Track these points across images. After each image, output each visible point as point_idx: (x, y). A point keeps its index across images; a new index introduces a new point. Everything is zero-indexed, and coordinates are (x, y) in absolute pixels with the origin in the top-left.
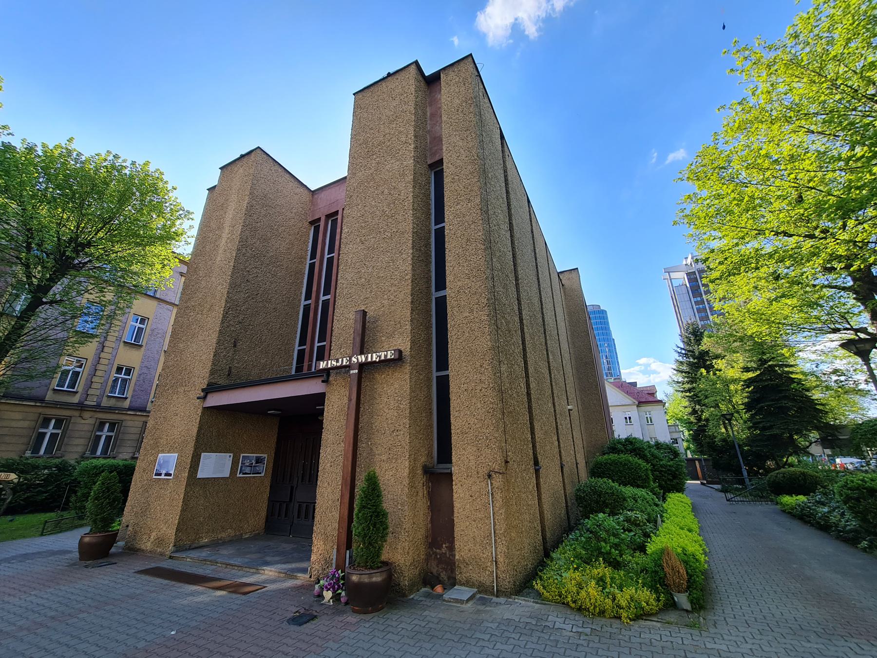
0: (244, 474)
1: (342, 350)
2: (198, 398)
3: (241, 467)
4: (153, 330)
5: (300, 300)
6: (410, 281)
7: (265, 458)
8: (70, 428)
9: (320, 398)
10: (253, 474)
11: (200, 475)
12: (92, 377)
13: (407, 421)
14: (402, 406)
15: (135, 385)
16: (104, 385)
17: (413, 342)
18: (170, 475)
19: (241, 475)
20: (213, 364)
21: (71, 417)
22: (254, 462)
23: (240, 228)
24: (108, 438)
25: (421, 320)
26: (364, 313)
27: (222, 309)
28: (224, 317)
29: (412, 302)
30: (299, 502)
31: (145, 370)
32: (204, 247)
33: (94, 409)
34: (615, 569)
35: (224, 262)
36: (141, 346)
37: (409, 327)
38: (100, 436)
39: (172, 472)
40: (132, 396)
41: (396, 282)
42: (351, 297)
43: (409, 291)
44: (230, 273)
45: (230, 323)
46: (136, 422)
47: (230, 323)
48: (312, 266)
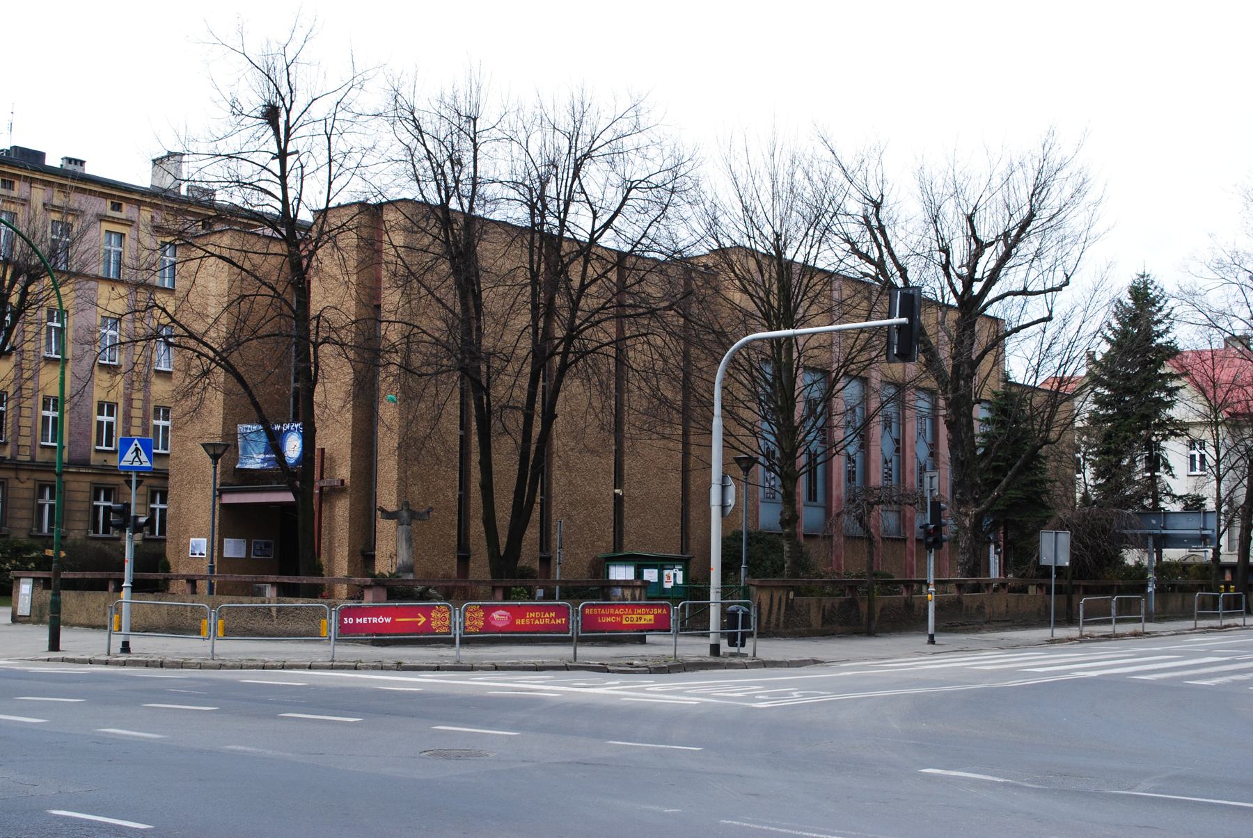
8: (9, 496)
11: (225, 555)
13: (348, 524)
15: (70, 425)
16: (33, 428)
17: (353, 473)
24: (52, 507)
28: (224, 423)
33: (30, 468)
34: (1045, 524)
38: (43, 505)
39: (205, 552)
40: (69, 444)
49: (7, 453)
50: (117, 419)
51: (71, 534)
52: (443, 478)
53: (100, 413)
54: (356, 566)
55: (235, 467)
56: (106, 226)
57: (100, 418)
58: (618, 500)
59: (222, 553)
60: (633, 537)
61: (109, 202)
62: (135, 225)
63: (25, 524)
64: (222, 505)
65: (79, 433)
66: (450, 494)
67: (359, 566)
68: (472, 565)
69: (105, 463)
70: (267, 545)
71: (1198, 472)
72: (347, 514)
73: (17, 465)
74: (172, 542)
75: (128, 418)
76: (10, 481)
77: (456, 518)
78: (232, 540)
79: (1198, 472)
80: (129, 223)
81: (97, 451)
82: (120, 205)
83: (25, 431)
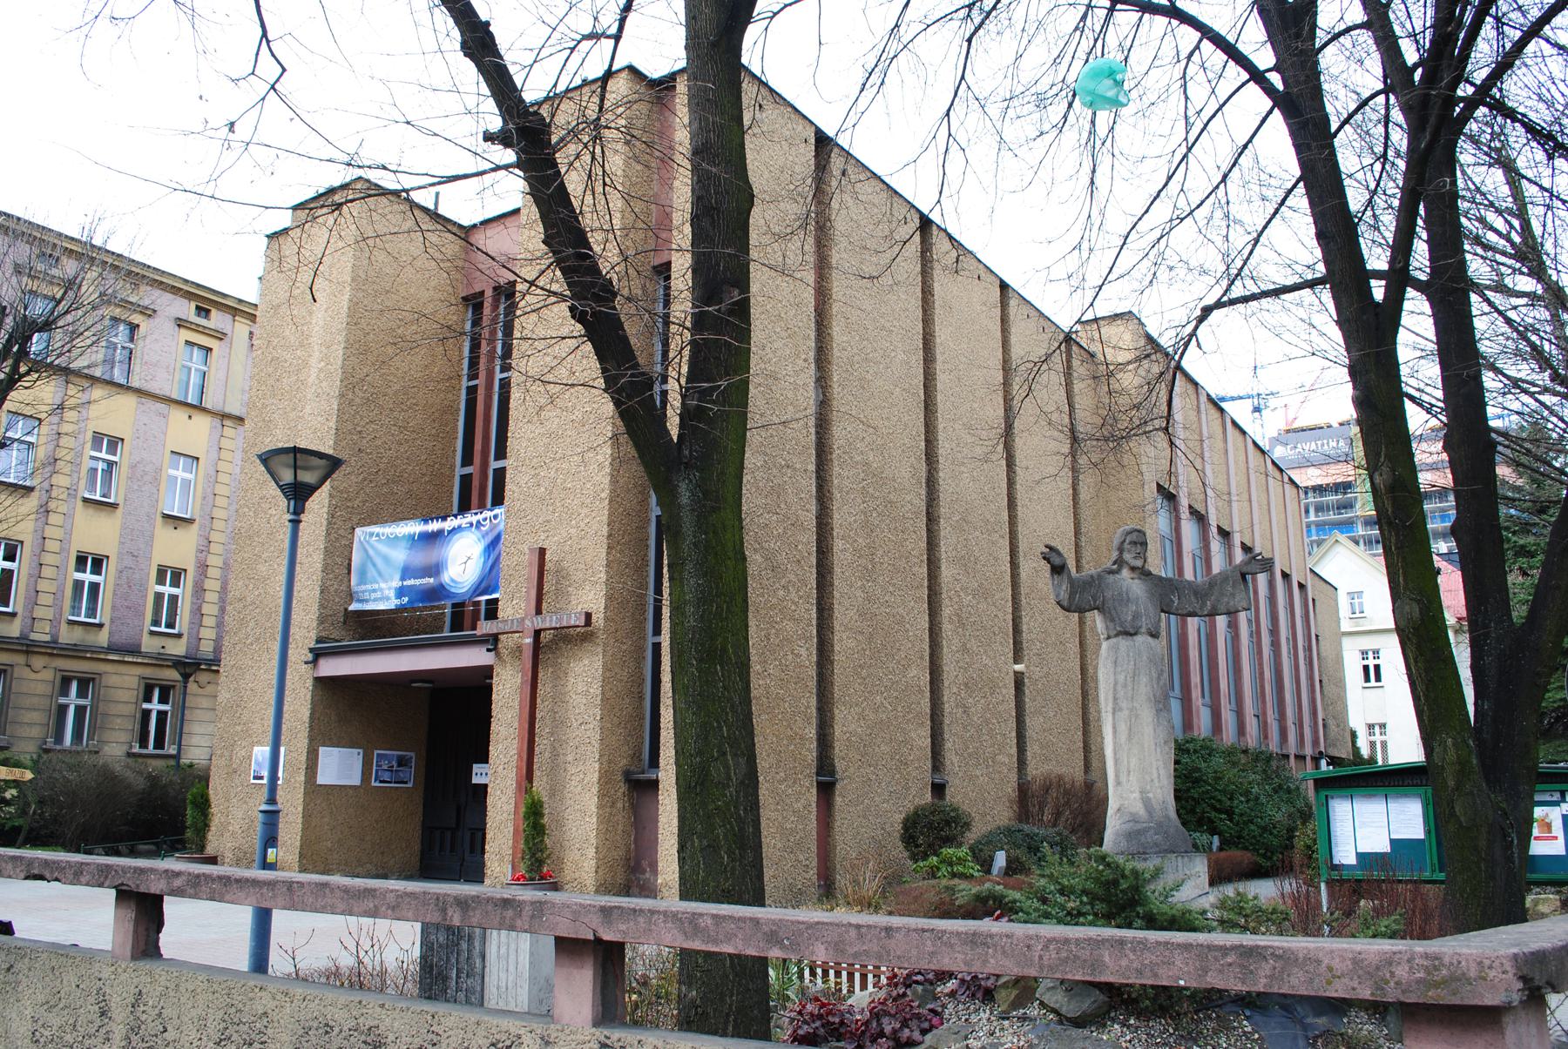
0: (381, 782)
1: (514, 602)
2: (306, 663)
3: (377, 771)
4: (133, 467)
5: (452, 468)
6: (607, 502)
7: (411, 758)
9: (487, 672)
10: (395, 783)
11: (321, 780)
12: (36, 582)
13: (598, 712)
14: (591, 690)
15: (115, 594)
18: (261, 778)
19: (377, 784)
20: (322, 606)
21: (12, 666)
22: (395, 764)
23: (341, 352)
24: (80, 711)
25: (627, 560)
26: (542, 552)
27: (326, 510)
28: (329, 523)
29: (610, 536)
30: (471, 829)
31: (128, 561)
32: (278, 380)
33: (49, 651)
35: (319, 419)
36: (114, 506)
37: (603, 576)
40: (112, 621)
41: (589, 501)
42: (525, 517)
43: (605, 519)
44: (331, 442)
45: (340, 532)
46: (126, 678)
47: (340, 532)
48: (472, 391)
49: (14, 629)
50: (184, 592)
51: (106, 748)
52: (792, 619)
53: (161, 581)
54: (613, 804)
55: (346, 609)
56: (186, 335)
57: (160, 588)
58: (1019, 681)
59: (315, 777)
60: (1036, 747)
61: (193, 305)
62: (227, 340)
63: (36, 732)
64: (323, 683)
65: (127, 607)
66: (803, 652)
67: (620, 805)
68: (838, 800)
69: (162, 651)
70: (402, 762)
71: (1373, 683)
72: (596, 689)
73: (28, 645)
74: (222, 756)
75: (199, 590)
76: (16, 669)
77: (814, 701)
78: (335, 750)
79: (1373, 683)
80: (220, 336)
81: (152, 633)
82: (208, 311)
83: (44, 599)
